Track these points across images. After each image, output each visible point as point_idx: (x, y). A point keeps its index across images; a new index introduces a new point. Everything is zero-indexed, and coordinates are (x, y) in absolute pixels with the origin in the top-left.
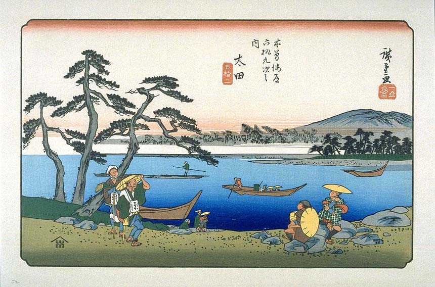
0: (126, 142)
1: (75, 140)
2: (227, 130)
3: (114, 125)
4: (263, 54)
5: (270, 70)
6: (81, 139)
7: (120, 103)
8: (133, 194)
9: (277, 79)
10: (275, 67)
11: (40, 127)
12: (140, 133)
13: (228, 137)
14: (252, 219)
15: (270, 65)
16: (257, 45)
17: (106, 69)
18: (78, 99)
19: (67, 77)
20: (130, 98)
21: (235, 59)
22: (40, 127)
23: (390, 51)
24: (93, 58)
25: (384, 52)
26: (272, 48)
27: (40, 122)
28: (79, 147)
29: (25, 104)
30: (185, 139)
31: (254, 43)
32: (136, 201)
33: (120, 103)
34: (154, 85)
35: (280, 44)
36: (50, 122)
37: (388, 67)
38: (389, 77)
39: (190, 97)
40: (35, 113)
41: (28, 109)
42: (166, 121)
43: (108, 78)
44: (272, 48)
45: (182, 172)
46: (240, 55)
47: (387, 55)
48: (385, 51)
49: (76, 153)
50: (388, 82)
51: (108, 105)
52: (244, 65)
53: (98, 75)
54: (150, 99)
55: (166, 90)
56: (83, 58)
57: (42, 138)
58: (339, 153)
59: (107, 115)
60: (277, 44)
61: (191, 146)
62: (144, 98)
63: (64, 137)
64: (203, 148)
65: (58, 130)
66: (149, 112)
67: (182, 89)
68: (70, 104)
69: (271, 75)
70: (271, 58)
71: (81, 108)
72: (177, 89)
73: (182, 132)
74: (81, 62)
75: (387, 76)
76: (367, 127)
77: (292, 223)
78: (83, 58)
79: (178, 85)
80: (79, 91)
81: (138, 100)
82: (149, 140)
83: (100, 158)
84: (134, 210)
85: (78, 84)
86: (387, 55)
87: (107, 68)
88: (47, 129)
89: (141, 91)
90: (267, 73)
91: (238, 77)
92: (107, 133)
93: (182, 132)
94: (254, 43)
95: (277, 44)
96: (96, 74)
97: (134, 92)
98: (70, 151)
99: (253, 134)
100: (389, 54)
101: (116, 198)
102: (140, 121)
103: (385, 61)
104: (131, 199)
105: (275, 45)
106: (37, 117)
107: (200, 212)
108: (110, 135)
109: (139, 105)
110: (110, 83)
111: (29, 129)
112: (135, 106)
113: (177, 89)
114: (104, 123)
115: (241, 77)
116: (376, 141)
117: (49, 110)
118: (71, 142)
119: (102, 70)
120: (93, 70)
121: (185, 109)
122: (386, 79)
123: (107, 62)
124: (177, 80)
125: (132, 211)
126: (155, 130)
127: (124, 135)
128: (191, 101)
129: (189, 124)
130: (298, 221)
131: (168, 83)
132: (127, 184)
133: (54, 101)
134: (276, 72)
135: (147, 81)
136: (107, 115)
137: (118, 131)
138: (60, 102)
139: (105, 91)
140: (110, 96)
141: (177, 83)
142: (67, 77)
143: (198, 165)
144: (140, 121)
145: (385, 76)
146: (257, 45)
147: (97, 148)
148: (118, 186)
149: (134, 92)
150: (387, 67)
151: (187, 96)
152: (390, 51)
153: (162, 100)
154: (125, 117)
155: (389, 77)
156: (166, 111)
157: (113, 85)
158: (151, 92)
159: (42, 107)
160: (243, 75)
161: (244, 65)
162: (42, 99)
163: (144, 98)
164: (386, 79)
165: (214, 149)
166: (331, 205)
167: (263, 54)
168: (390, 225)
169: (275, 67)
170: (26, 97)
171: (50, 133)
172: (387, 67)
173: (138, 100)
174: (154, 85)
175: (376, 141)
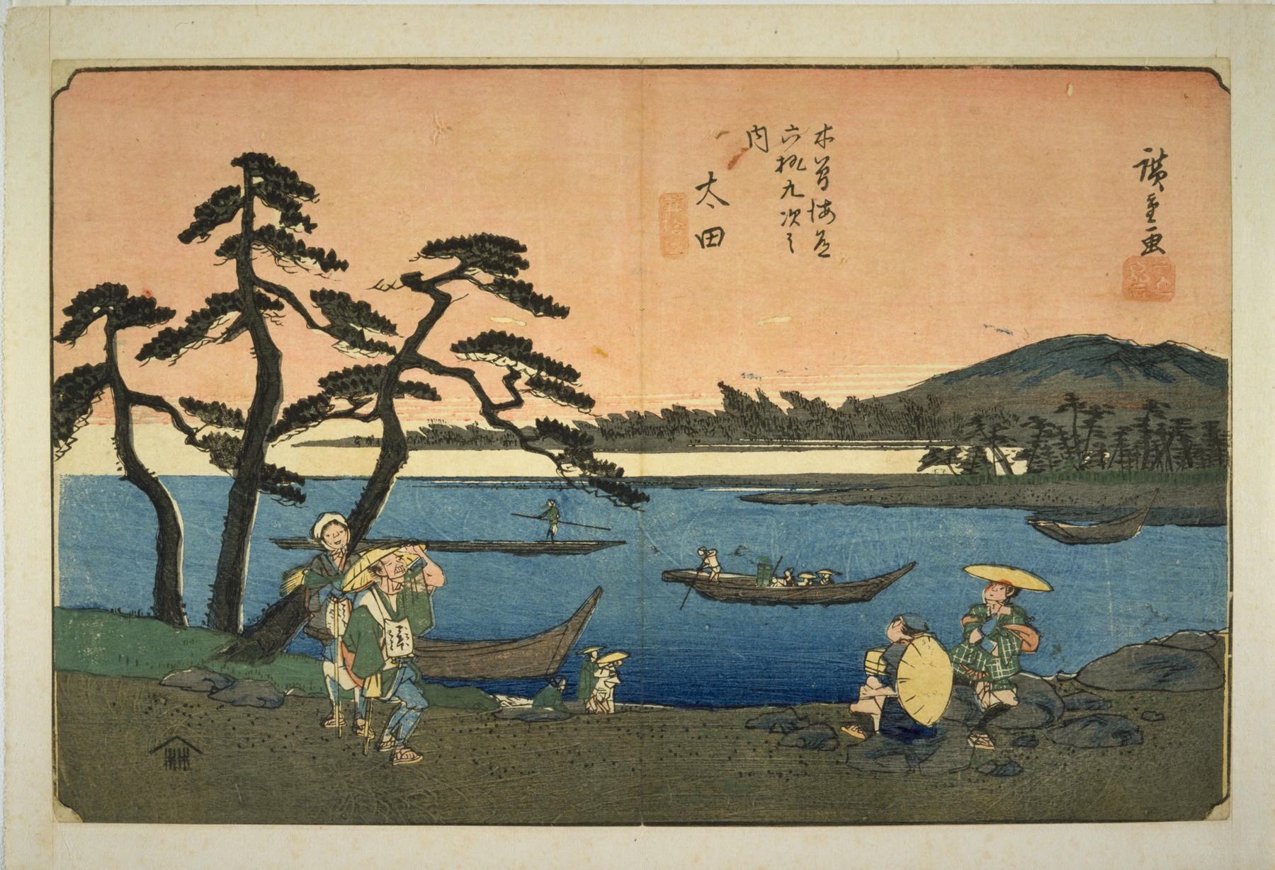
0: (370, 441)
1: (209, 430)
2: (675, 402)
3: (335, 383)
4: (780, 169)
5: (803, 218)
6: (221, 424)
7: (346, 317)
8: (393, 600)
9: (827, 128)
10: (818, 211)
11: (108, 393)
12: (412, 415)
13: (678, 428)
14: (760, 703)
15: (804, 205)
16: (761, 142)
17: (304, 211)
18: (219, 304)
19: (186, 237)
20: (382, 305)
21: (699, 188)
22: (108, 393)
23: (1163, 156)
24: (274, 180)
25: (1145, 162)
26: (808, 151)
27: (107, 374)
28: (218, 451)
29: (62, 320)
30: (548, 429)
31: (754, 136)
32: (405, 623)
33: (346, 317)
34: (454, 263)
35: (832, 139)
36: (136, 376)
37: (1157, 204)
38: (1160, 237)
39: (559, 300)
40: (89, 349)
41: (69, 334)
42: (491, 371)
43: (311, 241)
44: (808, 151)
45: (530, 532)
46: (711, 174)
47: (1154, 170)
48: (1148, 156)
49: (215, 471)
50: (1158, 253)
51: (312, 324)
52: (724, 203)
53: (282, 231)
54: (443, 302)
55: (486, 278)
56: (235, 177)
57: (111, 429)
58: (1010, 470)
59: (309, 358)
60: (823, 137)
61: (562, 452)
62: (425, 303)
63: (179, 424)
64: (600, 456)
65: (157, 403)
66: (435, 347)
67: (538, 277)
68: (195, 319)
69: (806, 232)
70: (806, 182)
71: (230, 334)
72: (523, 276)
73: (538, 408)
74: (226, 194)
75: (1154, 232)
76: (1093, 389)
77: (873, 681)
78: (235, 177)
79: (525, 265)
80: (226, 279)
81: (406, 310)
82: (441, 437)
83: (289, 487)
84: (397, 652)
85: (221, 259)
86: (1154, 170)
87: (306, 208)
88: (126, 400)
89: (413, 281)
90: (795, 230)
91: (706, 242)
92: (307, 413)
93: (538, 408)
94: (754, 136)
95: (823, 137)
96: (278, 227)
97: (391, 287)
98: (200, 464)
99: (746, 419)
100: (1160, 166)
101: (341, 613)
102: (411, 375)
103: (1149, 187)
104: (387, 616)
105: (817, 142)
106: (97, 357)
107: (595, 654)
108: (322, 416)
109: (407, 329)
110: (317, 254)
111: (71, 397)
112: (394, 327)
113: (523, 276)
114: (298, 384)
115: (715, 241)
116: (1118, 429)
117: (134, 338)
118: (199, 437)
119: (292, 216)
120: (267, 216)
121: (547, 338)
122: (1153, 243)
123: (309, 192)
124: (524, 249)
125: (391, 654)
126: (457, 406)
127: (366, 419)
128: (563, 312)
129: (557, 379)
130: (889, 679)
131: (495, 257)
132: (374, 569)
133: (143, 310)
134: (821, 224)
135: (432, 250)
136: (309, 358)
137: (341, 404)
138: (168, 314)
139: (303, 279)
140: (321, 297)
141: (523, 256)
142: (186, 237)
143: (593, 514)
144: (411, 375)
145: (1149, 234)
146: (761, 142)
147: (280, 454)
148: (350, 576)
149: (391, 287)
150: (1153, 204)
151: (550, 299)
152: (1163, 156)
153: (477, 308)
154: (359, 358)
155: (1160, 237)
156: (491, 342)
157: (330, 262)
158: (443, 288)
159: (110, 332)
160: (723, 234)
161: (724, 203)
162: (115, 305)
163: (425, 303)
164: (1153, 243)
165: (632, 464)
166: (988, 629)
167: (780, 169)
168: (1161, 686)
169: (818, 211)
170: (66, 298)
171: (137, 411)
172: (1153, 204)
173: (406, 310)
174: (454, 263)
175: (1122, 431)
